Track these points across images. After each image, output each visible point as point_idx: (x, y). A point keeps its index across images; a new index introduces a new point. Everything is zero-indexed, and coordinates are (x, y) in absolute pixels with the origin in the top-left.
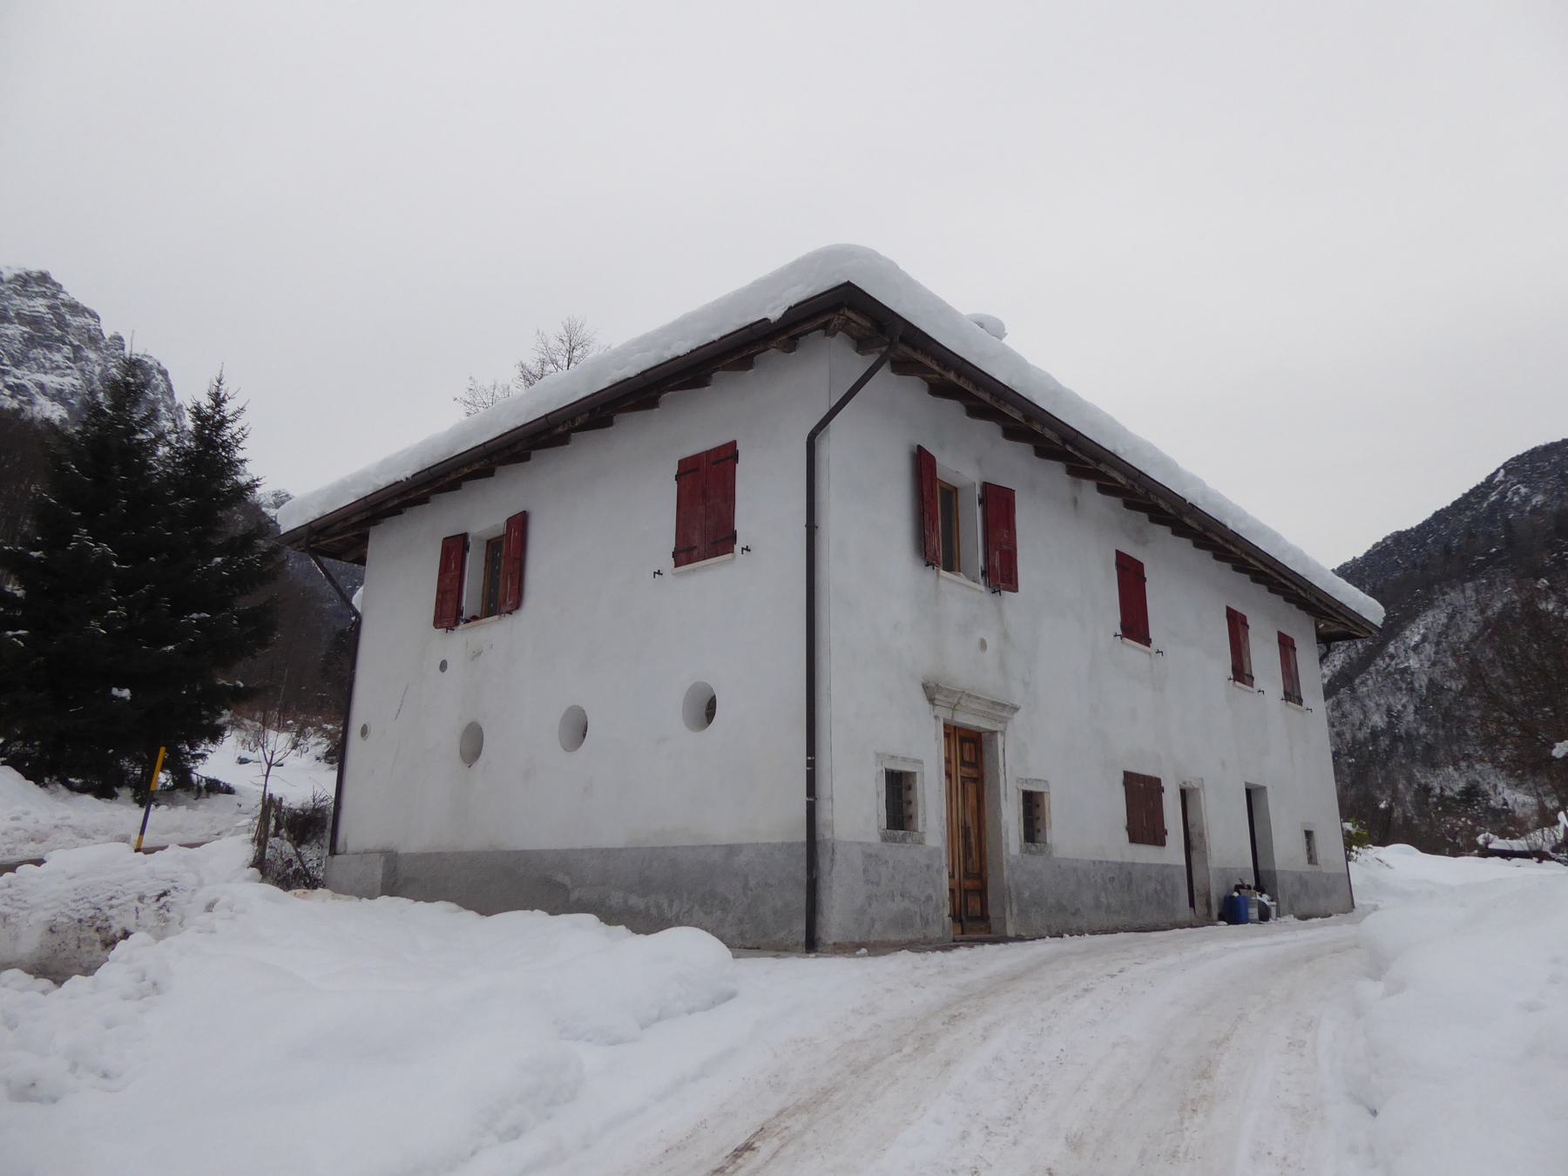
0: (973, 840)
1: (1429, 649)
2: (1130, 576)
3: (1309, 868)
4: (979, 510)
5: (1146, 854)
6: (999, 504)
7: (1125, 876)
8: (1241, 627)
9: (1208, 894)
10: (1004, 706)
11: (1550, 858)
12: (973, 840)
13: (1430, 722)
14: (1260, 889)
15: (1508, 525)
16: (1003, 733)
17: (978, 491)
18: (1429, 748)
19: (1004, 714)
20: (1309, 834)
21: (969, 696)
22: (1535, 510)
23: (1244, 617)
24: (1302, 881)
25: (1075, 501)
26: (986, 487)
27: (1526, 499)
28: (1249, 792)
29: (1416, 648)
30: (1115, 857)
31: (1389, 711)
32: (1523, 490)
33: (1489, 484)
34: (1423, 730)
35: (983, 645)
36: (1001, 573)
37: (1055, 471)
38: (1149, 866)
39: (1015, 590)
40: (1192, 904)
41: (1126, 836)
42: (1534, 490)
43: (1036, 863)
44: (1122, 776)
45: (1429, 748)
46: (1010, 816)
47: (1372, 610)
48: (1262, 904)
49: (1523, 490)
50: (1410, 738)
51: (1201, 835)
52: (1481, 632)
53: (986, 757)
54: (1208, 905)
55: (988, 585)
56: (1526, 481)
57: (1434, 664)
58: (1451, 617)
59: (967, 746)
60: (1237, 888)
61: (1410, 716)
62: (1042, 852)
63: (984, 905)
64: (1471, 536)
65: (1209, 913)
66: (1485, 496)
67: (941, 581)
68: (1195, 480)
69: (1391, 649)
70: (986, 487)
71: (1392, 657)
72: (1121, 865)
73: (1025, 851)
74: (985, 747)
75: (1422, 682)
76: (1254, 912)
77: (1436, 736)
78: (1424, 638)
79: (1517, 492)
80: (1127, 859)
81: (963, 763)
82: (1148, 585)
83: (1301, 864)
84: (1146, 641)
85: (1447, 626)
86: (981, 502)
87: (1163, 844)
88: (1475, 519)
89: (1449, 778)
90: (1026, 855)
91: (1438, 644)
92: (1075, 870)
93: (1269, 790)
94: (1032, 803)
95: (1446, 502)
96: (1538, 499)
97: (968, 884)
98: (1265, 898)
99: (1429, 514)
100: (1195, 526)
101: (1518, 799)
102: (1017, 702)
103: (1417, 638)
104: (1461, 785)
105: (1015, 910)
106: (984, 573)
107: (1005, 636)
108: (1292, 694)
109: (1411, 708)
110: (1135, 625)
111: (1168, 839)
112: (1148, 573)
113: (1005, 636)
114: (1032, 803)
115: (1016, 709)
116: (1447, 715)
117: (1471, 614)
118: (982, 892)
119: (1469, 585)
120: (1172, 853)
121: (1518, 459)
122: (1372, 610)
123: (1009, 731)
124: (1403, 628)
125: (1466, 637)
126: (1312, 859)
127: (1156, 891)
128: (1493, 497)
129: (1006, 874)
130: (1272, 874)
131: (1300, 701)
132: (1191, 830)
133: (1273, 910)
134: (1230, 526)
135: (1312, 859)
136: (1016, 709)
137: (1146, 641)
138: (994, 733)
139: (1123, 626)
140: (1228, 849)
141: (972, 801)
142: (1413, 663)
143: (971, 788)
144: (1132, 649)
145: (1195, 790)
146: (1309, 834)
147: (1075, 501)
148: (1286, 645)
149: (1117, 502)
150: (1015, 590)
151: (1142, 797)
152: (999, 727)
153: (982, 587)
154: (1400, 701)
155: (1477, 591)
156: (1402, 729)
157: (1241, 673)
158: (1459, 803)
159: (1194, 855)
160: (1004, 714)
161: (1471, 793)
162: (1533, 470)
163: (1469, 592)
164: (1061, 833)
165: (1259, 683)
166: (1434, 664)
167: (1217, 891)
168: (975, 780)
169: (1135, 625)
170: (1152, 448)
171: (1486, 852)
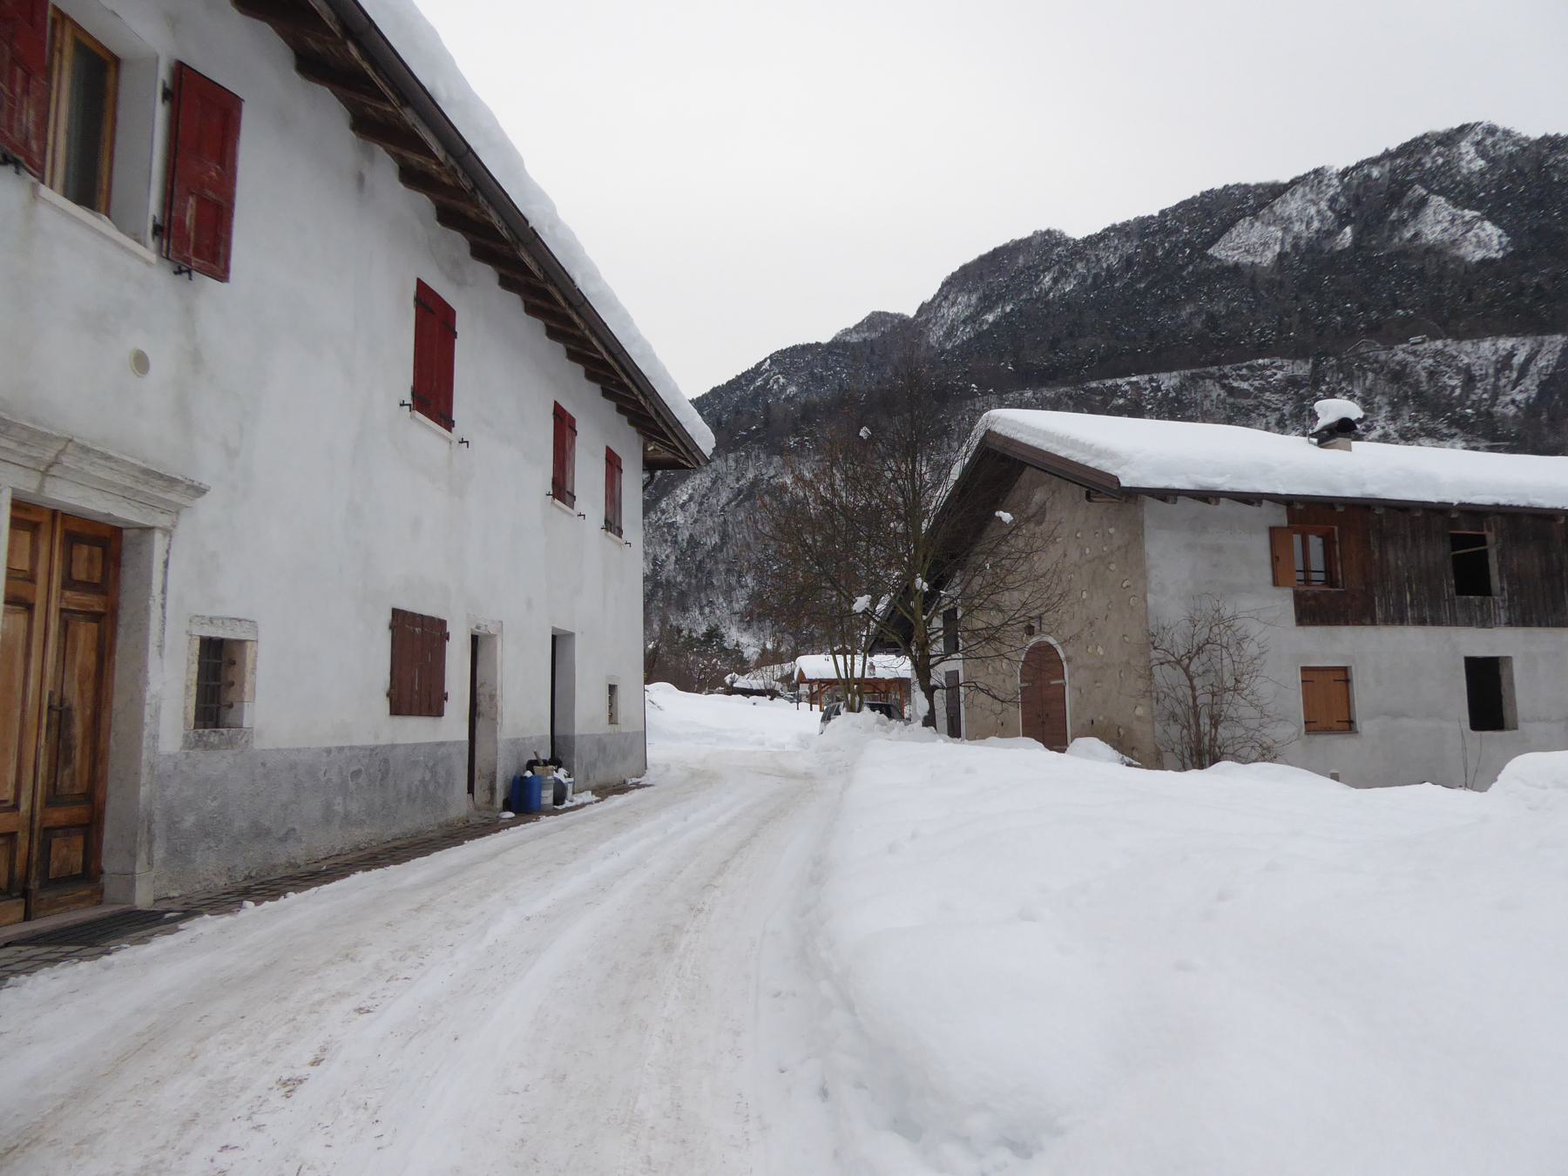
0: (78, 730)
1: (693, 507)
2: (434, 325)
3: (609, 729)
4: (160, 112)
5: (416, 730)
6: (205, 120)
7: (378, 766)
8: (568, 431)
9: (493, 775)
10: (172, 482)
11: (780, 696)
12: (78, 730)
13: (688, 574)
14: (555, 761)
15: (767, 407)
16: (168, 532)
17: (164, 74)
18: (682, 594)
19: (173, 497)
20: (612, 688)
21: (86, 450)
22: (789, 399)
23: (572, 420)
24: (601, 744)
25: (361, 179)
26: (181, 71)
27: (783, 388)
28: (554, 637)
29: (683, 506)
30: (364, 739)
31: (655, 559)
32: (782, 380)
33: (756, 371)
34: (679, 579)
35: (141, 363)
36: (197, 236)
37: (324, 113)
38: (416, 746)
39: (222, 275)
40: (471, 789)
41: (385, 705)
42: (790, 381)
43: (218, 762)
44: (389, 616)
45: (682, 594)
46: (166, 684)
47: (704, 437)
48: (558, 782)
49: (782, 380)
50: (669, 584)
51: (492, 697)
52: (735, 498)
53: (128, 575)
54: (492, 789)
55: (165, 254)
56: (785, 373)
57: (696, 521)
58: (714, 482)
59: (82, 552)
60: (531, 765)
61: (671, 566)
62: (230, 743)
63: (92, 851)
64: (738, 412)
65: (492, 801)
66: (753, 380)
67: (43, 211)
68: (542, 196)
69: (663, 505)
70: (181, 71)
71: (663, 512)
72: (373, 750)
73: (191, 744)
74: (127, 556)
75: (684, 535)
76: (547, 796)
77: (689, 584)
78: (691, 498)
79: (777, 381)
80: (384, 740)
81: (69, 583)
82: (458, 343)
83: (602, 726)
84: (448, 423)
85: (709, 489)
86: (167, 95)
87: (440, 714)
88: (742, 399)
89: (695, 621)
90: (199, 754)
91: (701, 504)
92: (293, 766)
93: (577, 637)
94: (219, 665)
95: (722, 380)
96: (792, 390)
97: (59, 816)
98: (561, 774)
99: (708, 390)
100: (534, 268)
101: (750, 644)
102: (204, 479)
103: (685, 497)
104: (703, 629)
105: (159, 854)
106: (158, 230)
107: (195, 359)
108: (612, 525)
109: (673, 558)
110: (432, 395)
111: (448, 707)
112: (460, 326)
113: (195, 359)
114: (219, 665)
115: (200, 491)
116: (700, 567)
117: (730, 480)
118: (90, 827)
119: (731, 455)
120: (452, 725)
121: (782, 352)
122: (704, 437)
123: (184, 526)
124: (675, 487)
125: (723, 500)
126: (612, 719)
127: (422, 781)
128: (759, 382)
129: (144, 791)
130: (569, 740)
131: (620, 533)
132: (480, 690)
133: (570, 788)
134: (579, 282)
135: (612, 719)
136: (200, 491)
137: (448, 423)
138: (147, 530)
139: (415, 393)
140: (522, 716)
141: (84, 655)
142: (680, 519)
143: (85, 633)
144: (423, 430)
145: (491, 637)
146: (612, 689)
147: (361, 179)
148: (613, 463)
149: (422, 203)
150: (222, 275)
151: (416, 646)
152: (162, 520)
153: (152, 257)
154: (665, 551)
155: (737, 461)
156: (663, 577)
157: (561, 490)
158: (702, 643)
159: (480, 724)
160: (173, 497)
161: (713, 634)
162: (792, 363)
163: (732, 463)
164: (274, 711)
165: (581, 504)
166: (696, 521)
167: (505, 769)
168: (96, 617)
169: (432, 395)
170: (490, 116)
171: (731, 691)
